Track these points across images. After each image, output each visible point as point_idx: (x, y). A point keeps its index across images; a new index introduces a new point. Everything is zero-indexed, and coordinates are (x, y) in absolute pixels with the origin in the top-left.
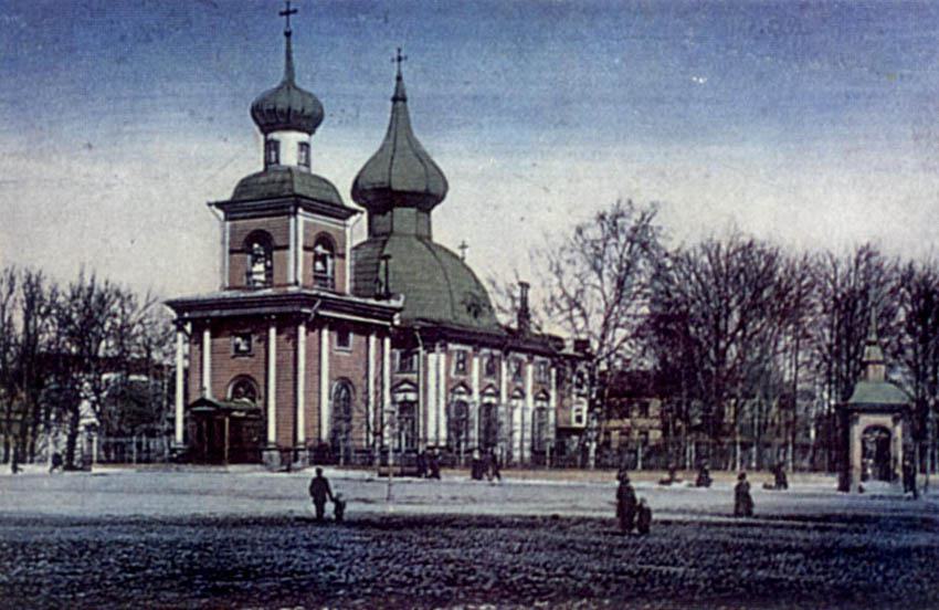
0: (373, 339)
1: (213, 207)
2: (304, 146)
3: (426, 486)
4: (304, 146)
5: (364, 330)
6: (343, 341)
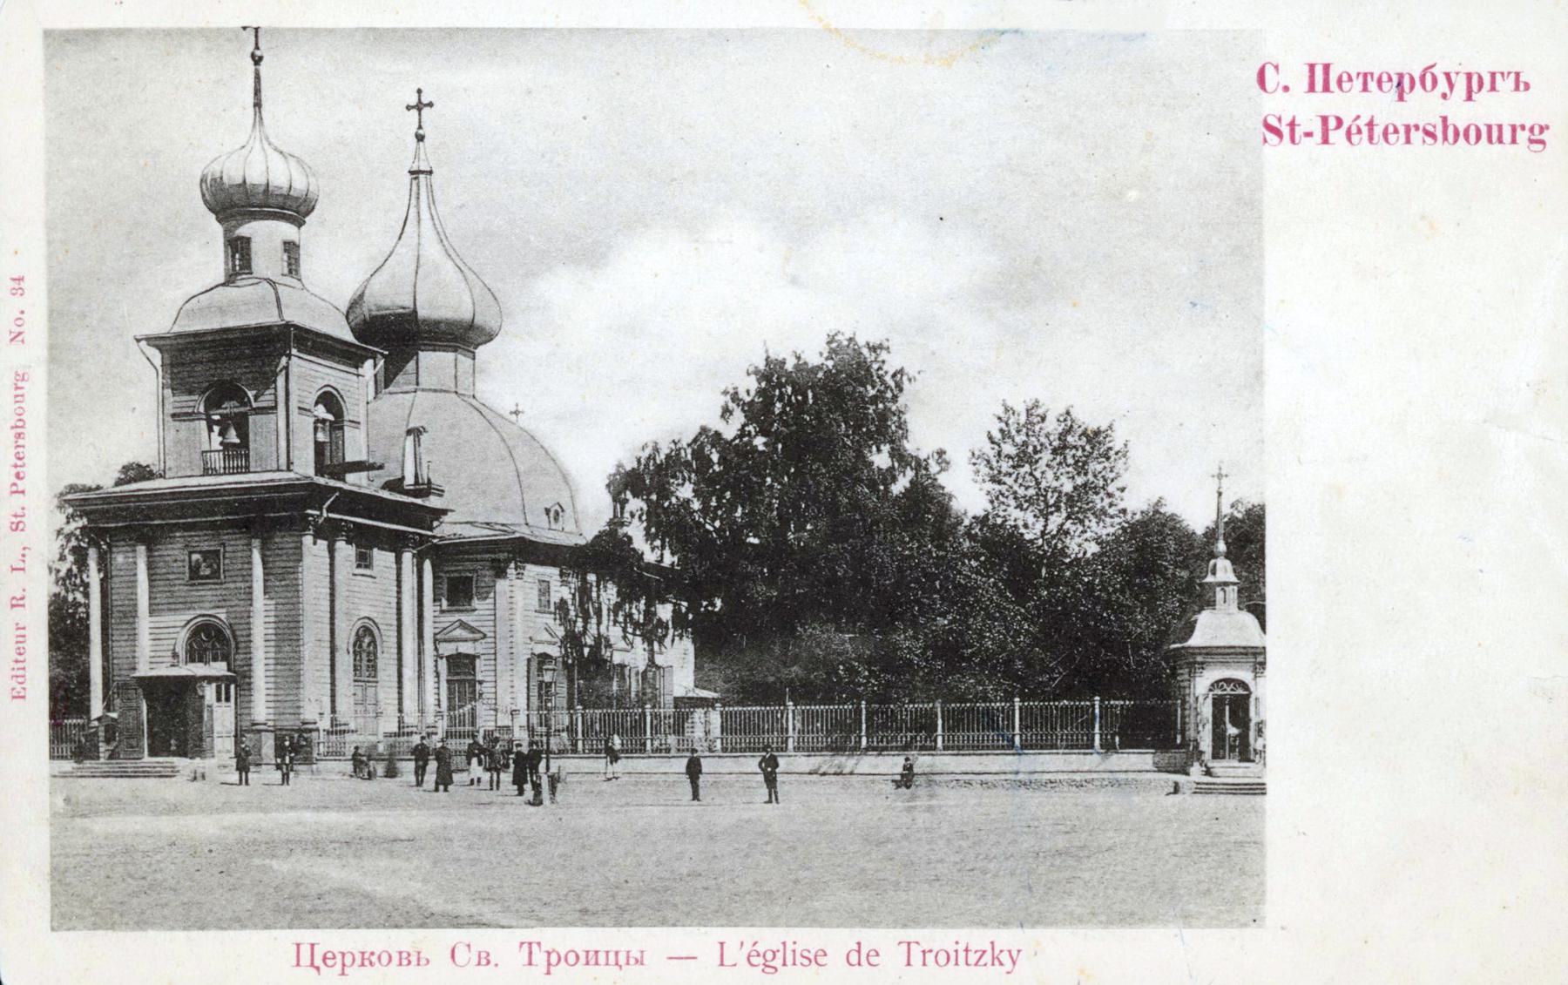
0: (407, 557)
1: (143, 343)
2: (291, 248)
3: (348, 783)
4: (291, 248)
5: (396, 544)
6: (364, 560)
